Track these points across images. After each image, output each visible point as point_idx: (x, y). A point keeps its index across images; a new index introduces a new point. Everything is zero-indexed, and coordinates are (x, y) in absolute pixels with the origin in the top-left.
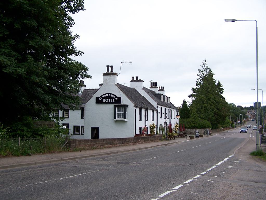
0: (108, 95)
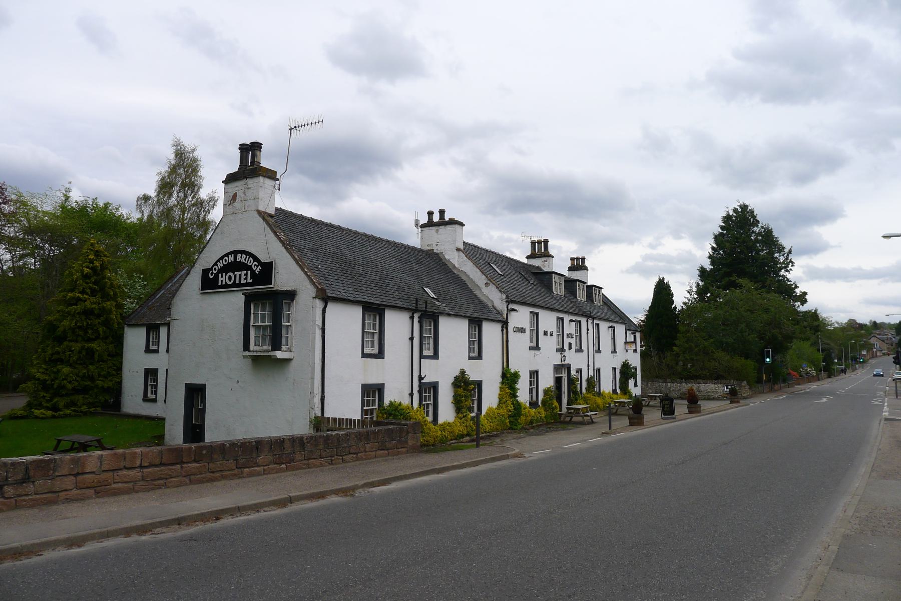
0: (235, 258)
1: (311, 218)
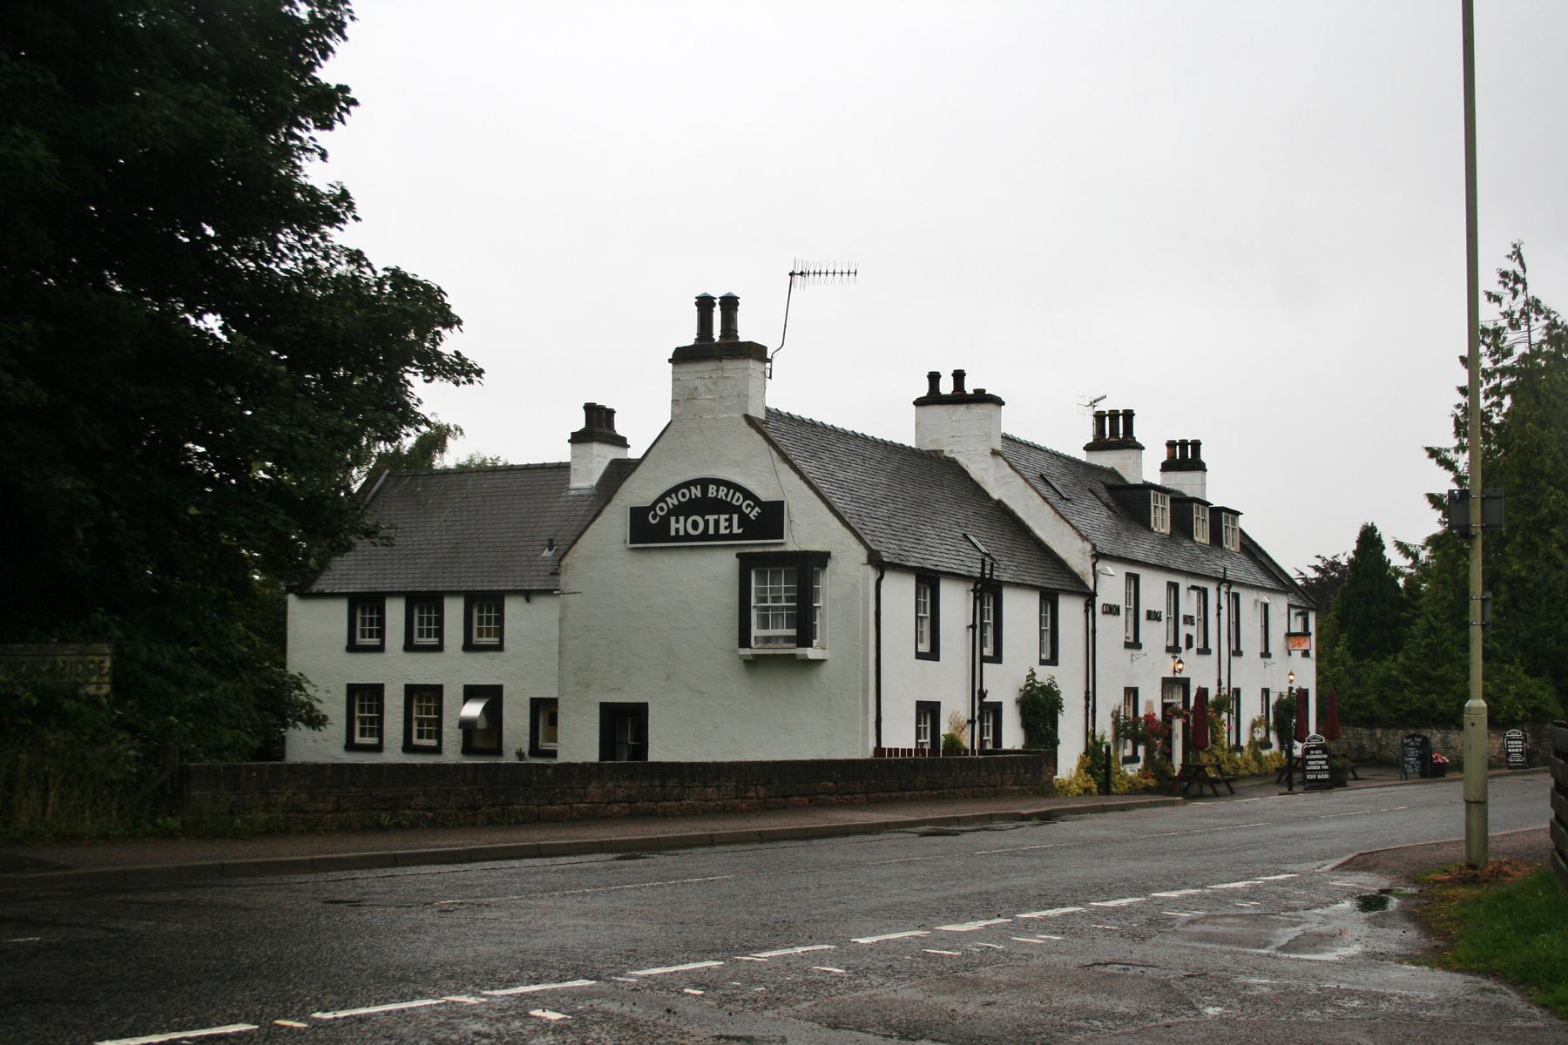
0: (705, 491)
1: (853, 431)
